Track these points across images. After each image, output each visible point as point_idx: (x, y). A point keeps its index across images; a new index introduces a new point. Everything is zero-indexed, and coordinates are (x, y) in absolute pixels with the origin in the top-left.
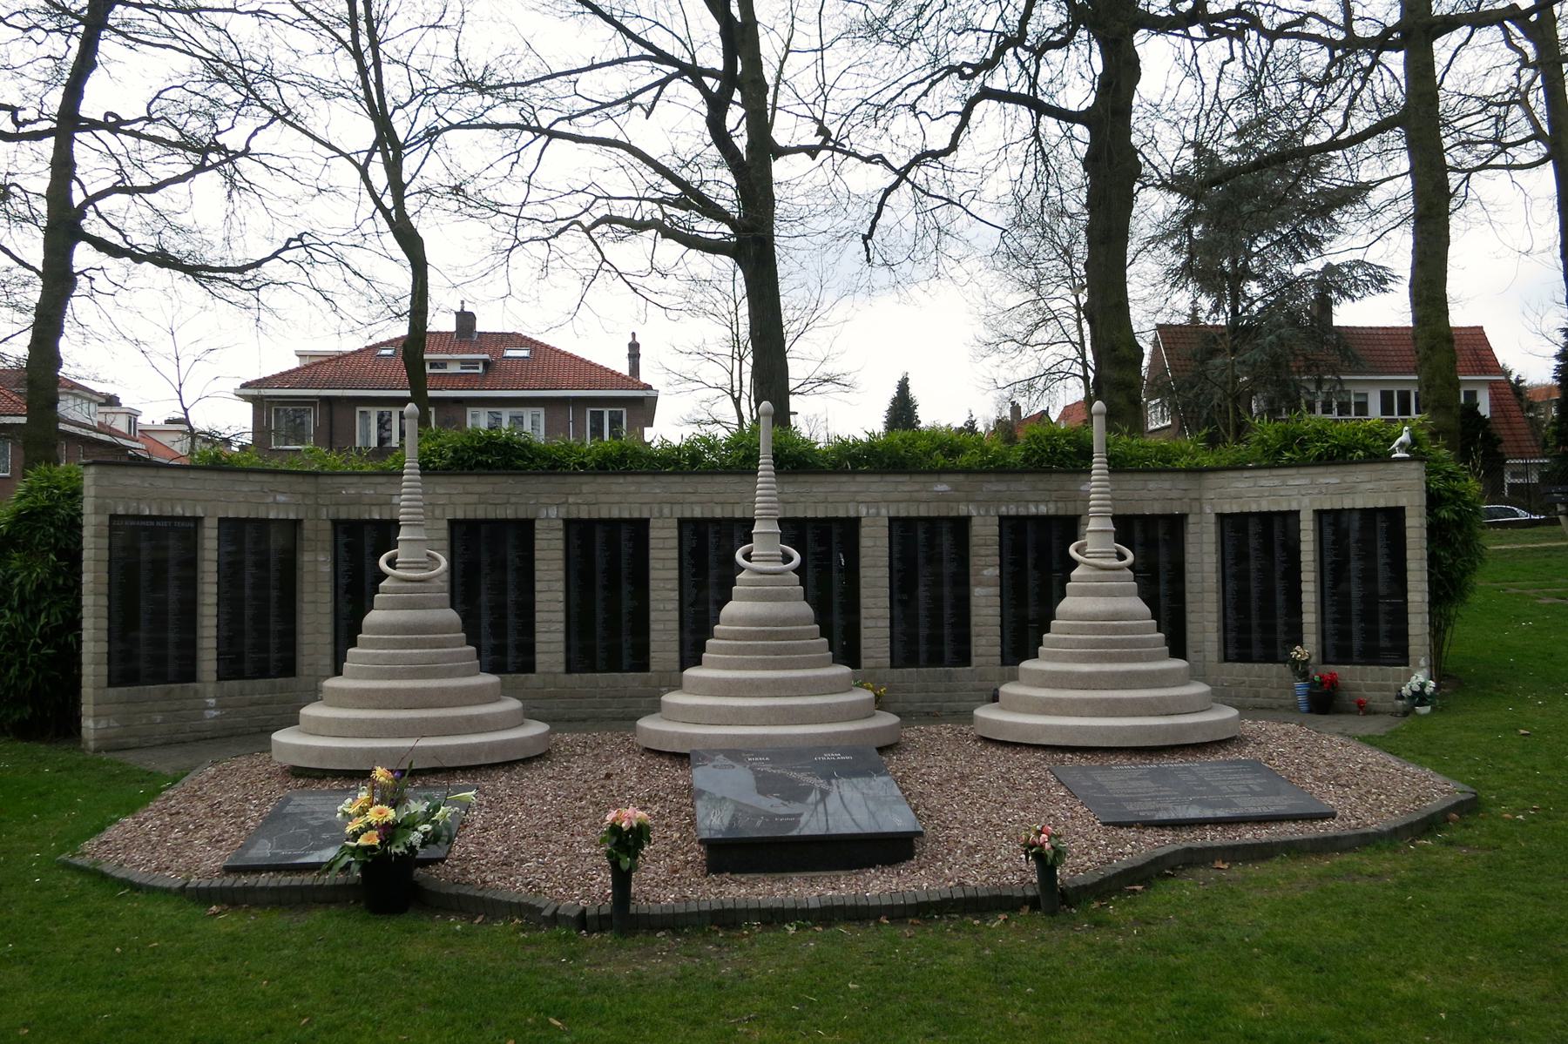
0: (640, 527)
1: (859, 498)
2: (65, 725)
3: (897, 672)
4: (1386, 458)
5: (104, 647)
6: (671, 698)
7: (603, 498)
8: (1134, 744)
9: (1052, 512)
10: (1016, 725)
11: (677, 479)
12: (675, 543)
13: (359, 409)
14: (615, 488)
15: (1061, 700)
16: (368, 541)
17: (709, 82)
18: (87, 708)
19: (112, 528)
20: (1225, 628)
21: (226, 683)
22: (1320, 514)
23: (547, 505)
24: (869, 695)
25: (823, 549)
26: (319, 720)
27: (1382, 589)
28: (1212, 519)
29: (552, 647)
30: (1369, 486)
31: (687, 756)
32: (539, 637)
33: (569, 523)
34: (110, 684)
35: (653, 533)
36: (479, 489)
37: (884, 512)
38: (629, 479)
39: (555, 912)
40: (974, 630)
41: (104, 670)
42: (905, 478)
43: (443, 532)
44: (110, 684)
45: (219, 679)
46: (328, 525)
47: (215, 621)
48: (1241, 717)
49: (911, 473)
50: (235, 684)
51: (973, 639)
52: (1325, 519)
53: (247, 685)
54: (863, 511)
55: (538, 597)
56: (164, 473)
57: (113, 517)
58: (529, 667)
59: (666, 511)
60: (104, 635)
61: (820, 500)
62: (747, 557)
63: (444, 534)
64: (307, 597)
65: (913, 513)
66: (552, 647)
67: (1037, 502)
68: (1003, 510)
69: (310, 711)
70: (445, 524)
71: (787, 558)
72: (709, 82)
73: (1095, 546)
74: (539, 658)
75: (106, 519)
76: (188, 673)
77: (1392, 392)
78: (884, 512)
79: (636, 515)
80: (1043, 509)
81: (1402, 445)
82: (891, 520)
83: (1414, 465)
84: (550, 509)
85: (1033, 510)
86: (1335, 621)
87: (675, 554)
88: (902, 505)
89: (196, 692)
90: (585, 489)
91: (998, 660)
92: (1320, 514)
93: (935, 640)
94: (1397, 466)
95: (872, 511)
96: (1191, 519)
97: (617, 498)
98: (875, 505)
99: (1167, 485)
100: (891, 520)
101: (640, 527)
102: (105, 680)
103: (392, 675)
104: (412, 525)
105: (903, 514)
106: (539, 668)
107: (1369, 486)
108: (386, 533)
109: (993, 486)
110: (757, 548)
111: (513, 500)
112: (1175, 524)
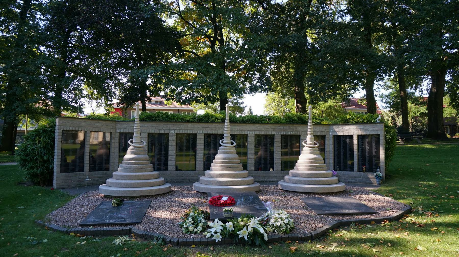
0: (195, 135)
1: (121, 128)
2: (50, 182)
3: (256, 172)
4: (375, 123)
5: (60, 163)
6: (202, 178)
7: (185, 128)
8: (320, 192)
9: (294, 134)
10: (290, 186)
11: (204, 124)
12: (203, 139)
13: (132, 111)
14: (189, 126)
15: (301, 180)
16: (218, 138)
17: (212, 39)
18: (55, 178)
19: (63, 133)
20: (334, 163)
21: (92, 172)
22: (358, 136)
23: (172, 130)
24: (252, 178)
25: (240, 141)
26: (111, 183)
27: (374, 154)
28: (332, 136)
29: (173, 164)
30: (371, 129)
31: (207, 193)
32: (169, 162)
33: (177, 134)
34: (61, 172)
35: (198, 137)
36: (155, 126)
37: (253, 133)
38: (192, 124)
39: (170, 240)
40: (275, 162)
41: (59, 169)
42: (259, 125)
43: (146, 136)
44: (61, 172)
45: (89, 171)
46: (118, 134)
47: (89, 157)
48: (346, 185)
49: (260, 124)
50: (94, 173)
51: (275, 164)
52: (360, 137)
53: (97, 173)
54: (248, 133)
55: (169, 152)
56: (76, 120)
57: (63, 131)
58: (167, 169)
59: (201, 132)
60: (60, 160)
61: (240, 129)
62: (222, 142)
63: (147, 136)
64: (112, 151)
65: (261, 134)
66: (173, 164)
67: (290, 132)
68: (282, 133)
69: (109, 180)
70: (147, 134)
71: (232, 143)
72: (212, 39)
73: (227, 139)
74: (169, 167)
75: (61, 131)
76: (82, 170)
77: (165, 136)
78: (253, 133)
79: (194, 133)
80: (292, 133)
81: (379, 120)
82: (255, 135)
83: (382, 124)
84: (172, 130)
85: (289, 133)
86: (362, 161)
87: (203, 142)
88: (258, 132)
89: (83, 174)
90: (181, 126)
91: (280, 169)
92: (358, 136)
93: (265, 164)
94: (378, 124)
95: (251, 133)
96: (327, 136)
97: (189, 128)
98: (251, 131)
99: (321, 128)
100: (255, 135)
101: (195, 135)
102: (60, 171)
103: (130, 171)
104: (137, 133)
105: (258, 134)
106: (169, 169)
107: (371, 129)
108: (130, 136)
109: (280, 127)
110: (225, 140)
111: (185, 128)
112: (245, 137)
